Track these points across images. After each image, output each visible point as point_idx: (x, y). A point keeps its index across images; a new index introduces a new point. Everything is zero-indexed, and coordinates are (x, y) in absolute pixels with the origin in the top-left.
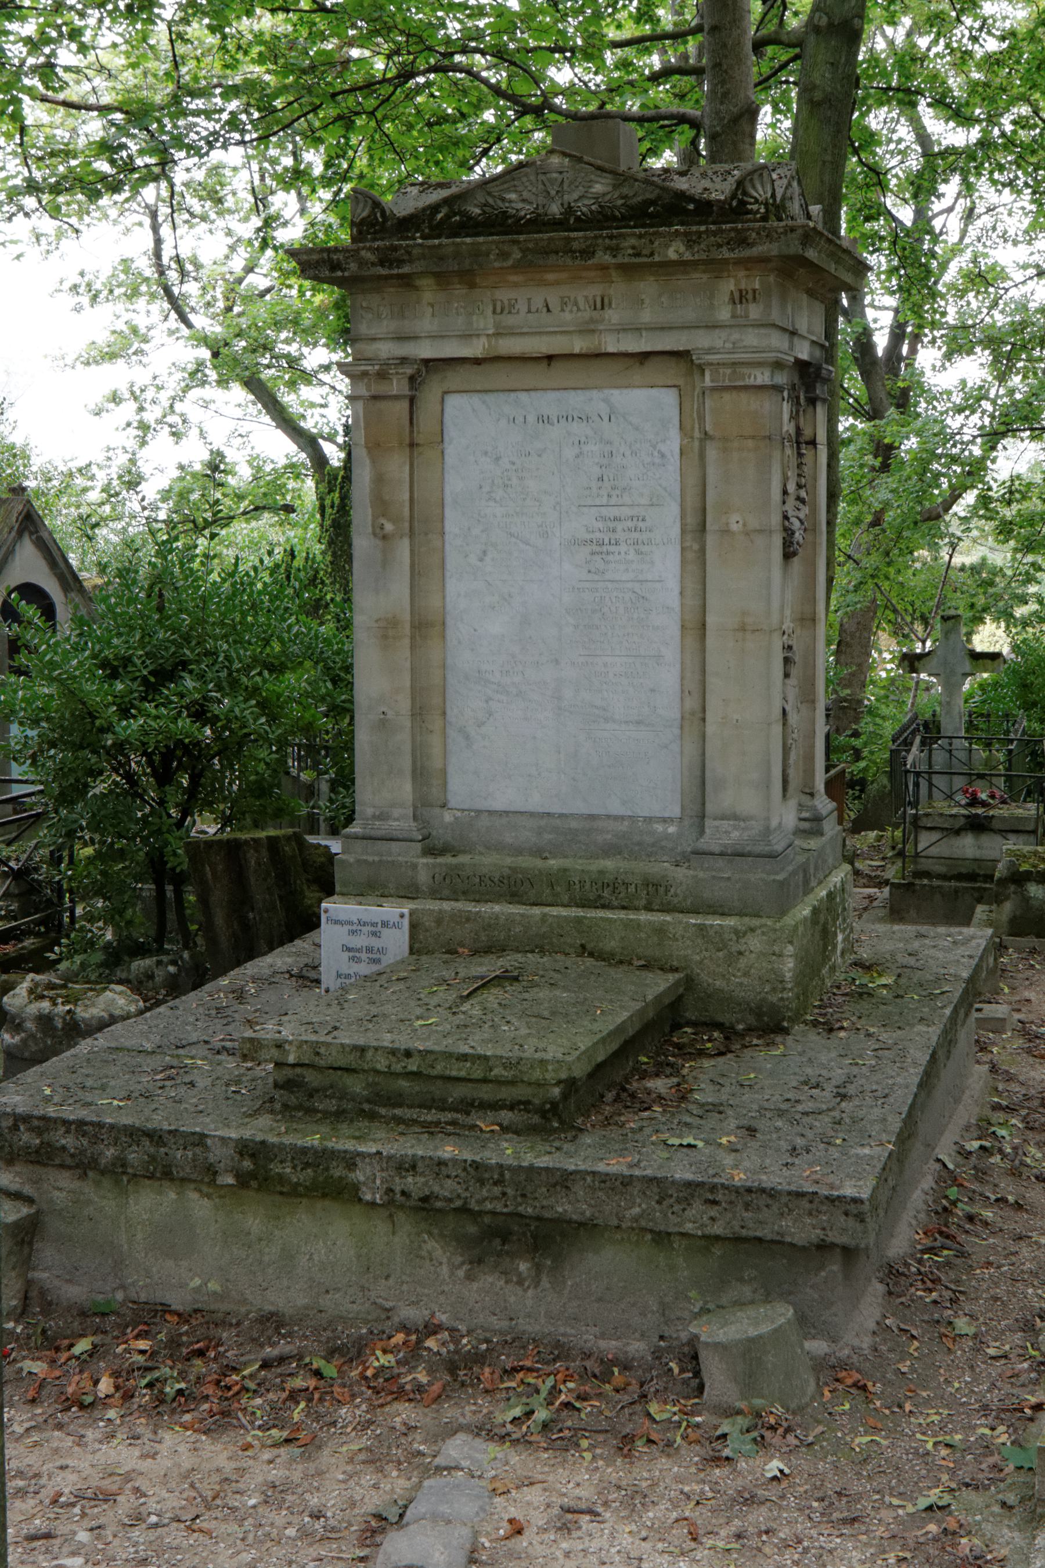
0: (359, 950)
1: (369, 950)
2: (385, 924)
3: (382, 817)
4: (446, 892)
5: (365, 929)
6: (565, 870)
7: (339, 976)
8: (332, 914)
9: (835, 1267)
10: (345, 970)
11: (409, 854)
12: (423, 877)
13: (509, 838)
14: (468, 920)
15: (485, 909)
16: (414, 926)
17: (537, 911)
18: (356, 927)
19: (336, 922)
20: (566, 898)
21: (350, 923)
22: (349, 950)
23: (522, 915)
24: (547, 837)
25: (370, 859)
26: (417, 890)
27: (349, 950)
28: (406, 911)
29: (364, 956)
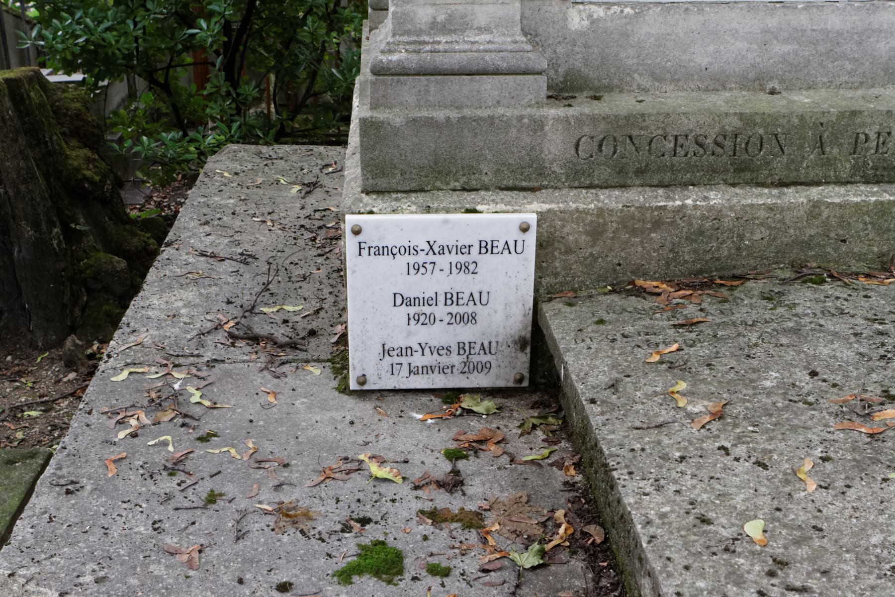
0: (427, 302)
1: (452, 298)
2: (487, 247)
3: (452, 25)
4: (603, 173)
5: (443, 261)
6: (854, 113)
7: (386, 351)
8: (370, 237)
9: (335, 384)
10: (399, 341)
11: (523, 100)
12: (555, 147)
13: (701, 56)
14: (657, 224)
15: (690, 199)
16: (545, 246)
17: (796, 197)
18: (421, 257)
19: (381, 251)
20: (845, 168)
21: (409, 250)
22: (408, 302)
23: (770, 208)
24: (779, 49)
25: (440, 115)
26: (541, 172)
27: (408, 302)
28: (532, 218)
29: (441, 311)
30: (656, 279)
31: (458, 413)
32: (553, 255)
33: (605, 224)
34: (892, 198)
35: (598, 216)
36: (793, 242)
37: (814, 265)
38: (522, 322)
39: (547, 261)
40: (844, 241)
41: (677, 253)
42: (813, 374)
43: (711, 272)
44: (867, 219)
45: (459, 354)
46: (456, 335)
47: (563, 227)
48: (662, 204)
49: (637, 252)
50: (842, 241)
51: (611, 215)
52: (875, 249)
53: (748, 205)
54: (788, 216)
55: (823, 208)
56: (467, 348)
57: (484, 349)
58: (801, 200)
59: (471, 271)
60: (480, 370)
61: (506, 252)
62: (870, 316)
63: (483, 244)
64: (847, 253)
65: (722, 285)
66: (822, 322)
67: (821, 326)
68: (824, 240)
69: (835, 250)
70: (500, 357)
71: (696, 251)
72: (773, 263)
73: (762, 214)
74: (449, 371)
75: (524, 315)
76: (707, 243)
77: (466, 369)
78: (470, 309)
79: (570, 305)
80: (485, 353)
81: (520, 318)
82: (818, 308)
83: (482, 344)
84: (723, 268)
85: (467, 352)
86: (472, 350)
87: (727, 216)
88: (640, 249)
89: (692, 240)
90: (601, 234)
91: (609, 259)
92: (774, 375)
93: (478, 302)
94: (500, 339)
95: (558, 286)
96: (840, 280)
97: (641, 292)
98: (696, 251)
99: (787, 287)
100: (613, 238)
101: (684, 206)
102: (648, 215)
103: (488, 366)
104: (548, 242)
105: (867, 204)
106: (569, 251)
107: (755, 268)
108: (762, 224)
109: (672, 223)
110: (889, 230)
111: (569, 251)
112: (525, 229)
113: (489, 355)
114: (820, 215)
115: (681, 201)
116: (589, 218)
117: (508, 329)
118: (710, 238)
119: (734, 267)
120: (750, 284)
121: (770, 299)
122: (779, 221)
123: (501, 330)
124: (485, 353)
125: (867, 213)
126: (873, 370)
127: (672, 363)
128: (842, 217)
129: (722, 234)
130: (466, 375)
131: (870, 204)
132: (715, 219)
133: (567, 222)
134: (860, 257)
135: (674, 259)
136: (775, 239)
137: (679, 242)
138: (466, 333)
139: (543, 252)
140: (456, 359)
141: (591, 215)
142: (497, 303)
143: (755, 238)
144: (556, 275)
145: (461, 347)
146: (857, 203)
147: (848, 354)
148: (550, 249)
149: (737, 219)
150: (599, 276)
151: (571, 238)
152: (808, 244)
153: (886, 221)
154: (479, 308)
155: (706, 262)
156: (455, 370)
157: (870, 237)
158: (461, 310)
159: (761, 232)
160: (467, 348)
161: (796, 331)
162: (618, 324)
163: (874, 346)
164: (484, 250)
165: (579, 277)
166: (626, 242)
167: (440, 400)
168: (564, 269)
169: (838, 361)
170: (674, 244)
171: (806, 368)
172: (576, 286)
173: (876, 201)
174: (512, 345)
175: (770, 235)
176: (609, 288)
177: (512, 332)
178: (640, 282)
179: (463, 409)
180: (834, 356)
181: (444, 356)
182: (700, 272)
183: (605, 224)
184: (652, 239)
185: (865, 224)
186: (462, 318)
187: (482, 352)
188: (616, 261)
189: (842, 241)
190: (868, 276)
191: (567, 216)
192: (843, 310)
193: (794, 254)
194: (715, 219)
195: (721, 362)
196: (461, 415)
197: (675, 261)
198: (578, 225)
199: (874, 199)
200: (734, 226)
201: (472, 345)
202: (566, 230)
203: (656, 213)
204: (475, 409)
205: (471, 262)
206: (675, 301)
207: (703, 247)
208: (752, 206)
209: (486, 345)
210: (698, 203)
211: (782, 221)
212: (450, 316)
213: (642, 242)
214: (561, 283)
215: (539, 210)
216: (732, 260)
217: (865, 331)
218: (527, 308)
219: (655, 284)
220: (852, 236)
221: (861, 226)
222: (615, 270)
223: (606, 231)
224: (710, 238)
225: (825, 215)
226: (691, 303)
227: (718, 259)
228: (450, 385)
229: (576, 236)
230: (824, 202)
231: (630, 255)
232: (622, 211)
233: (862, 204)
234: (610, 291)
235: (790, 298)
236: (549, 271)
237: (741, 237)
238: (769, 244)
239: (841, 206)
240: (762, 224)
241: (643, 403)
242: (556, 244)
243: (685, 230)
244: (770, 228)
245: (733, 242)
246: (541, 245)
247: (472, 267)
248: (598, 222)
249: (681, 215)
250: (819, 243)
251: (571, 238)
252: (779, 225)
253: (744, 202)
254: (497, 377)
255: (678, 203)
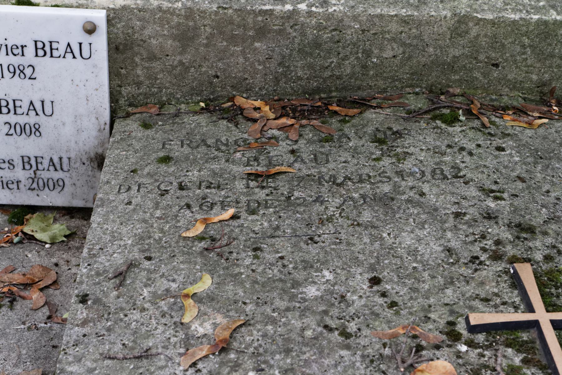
2: (44, 49)
14: (262, 32)
23: (405, 21)
30: (258, 96)
31: (16, 240)
32: (133, 61)
33: (196, 28)
34: (558, 18)
35: (187, 17)
36: (432, 62)
37: (458, 91)
38: (96, 137)
39: (126, 68)
40: (496, 65)
41: (288, 67)
42: (375, 281)
43: (331, 92)
44: (526, 41)
45: (24, 169)
46: (17, 148)
47: (143, 28)
48: (268, 7)
49: (237, 62)
50: (493, 65)
51: (204, 18)
52: (535, 77)
53: (377, 16)
54: (427, 32)
55: (471, 24)
56: (33, 162)
57: (54, 165)
58: (444, 13)
59: (28, 76)
60: (51, 187)
61: (69, 56)
62: (489, 185)
63: (40, 45)
64: (499, 80)
65: (336, 113)
66: (426, 188)
67: (422, 194)
68: (471, 63)
69: (485, 75)
70: (74, 174)
71: (311, 66)
72: (407, 86)
73: (394, 27)
74: (15, 186)
75: (99, 130)
76: (325, 58)
77: (35, 185)
78: (32, 119)
79: (146, 126)
80: (56, 170)
81: (94, 133)
82: (431, 162)
83: (51, 160)
84: (345, 88)
85: (34, 167)
86: (39, 165)
87: (350, 27)
88: (241, 60)
89: (307, 53)
90: (192, 39)
91: (204, 69)
92: (328, 275)
93: (40, 112)
94: (73, 155)
95: (141, 97)
96: (478, 118)
97: (235, 115)
98: (311, 66)
99: (408, 125)
100: (207, 46)
101: (295, 12)
102: (250, 20)
103: (61, 183)
104: (126, 45)
105: (527, 22)
106: (152, 57)
107: (385, 91)
108: (394, 39)
109: (281, 32)
110: (552, 56)
111: (152, 57)
112: (90, 29)
113: (61, 172)
114: (467, 33)
115: (292, 4)
116: (176, 19)
117: (81, 144)
118: (329, 52)
119: (359, 88)
120: (370, 114)
121: (381, 142)
122: (415, 37)
123: (73, 144)
124: (56, 170)
125: (526, 34)
126: (452, 283)
127: (213, 239)
128: (495, 36)
129: (344, 48)
130: (35, 192)
131: (530, 23)
132: (335, 30)
133: (148, 22)
134: (514, 86)
135: (284, 74)
136: (410, 58)
137: (290, 55)
138: (30, 146)
139: (120, 57)
140: (20, 174)
141: (178, 15)
142: (64, 113)
143: (385, 56)
144: (139, 84)
145: (26, 161)
146: (514, 22)
147: (432, 249)
148: (129, 54)
149: (363, 31)
150: (193, 89)
151: (154, 42)
152: (451, 67)
153: (550, 45)
154: (42, 119)
155: (325, 80)
156: (21, 186)
157: (529, 62)
158: (22, 120)
159: (393, 49)
160: (33, 162)
161: (386, 202)
162: (184, 165)
163: (471, 238)
164: (41, 53)
165: (167, 88)
166: (224, 51)
167: (6, 218)
168: (149, 78)
169: (416, 261)
170: (284, 57)
171: (372, 268)
172: (164, 98)
173: (538, 20)
174: (87, 163)
175: (404, 53)
176: (202, 104)
177: (87, 148)
178: (240, 101)
179: (25, 234)
180: (416, 250)
181: (7, 169)
182: (313, 92)
183: (196, 28)
184: (256, 49)
185: (523, 46)
186: (23, 129)
187: (52, 168)
188: (212, 72)
189: (493, 65)
190: (520, 111)
191: (147, 15)
192: (460, 170)
193: (433, 77)
194: (335, 30)
195: (273, 245)
196: (20, 242)
197: (285, 76)
198: (162, 26)
199: (536, 17)
200: (358, 40)
201: (39, 160)
202: (147, 32)
203: (260, 18)
204: (38, 236)
205: (26, 65)
206: (271, 133)
207: (320, 62)
208: (381, 16)
209: (56, 160)
210: (314, 9)
211: (419, 37)
212: (8, 126)
213: (243, 52)
214: (146, 94)
215: (112, 6)
216: (356, 79)
217: (471, 211)
218: (102, 123)
219: (258, 103)
220: (506, 60)
221: (518, 49)
222: (211, 83)
223: (198, 36)
224: (329, 52)
225: (474, 32)
226: (287, 138)
227: (339, 78)
228: (18, 202)
229: (160, 40)
230: (473, 17)
231: (229, 66)
232: (216, 13)
233: (521, 22)
234: (202, 109)
235: (406, 144)
236: (130, 79)
237: (368, 54)
238: (402, 64)
239: (494, 24)
240: (394, 39)
241: (143, 310)
242: (136, 49)
243: (297, 41)
244: (404, 44)
245: (358, 58)
246: (116, 49)
247: (28, 71)
248: (187, 25)
249: (292, 22)
250: (464, 66)
251: (154, 42)
252: (415, 42)
253: (371, 11)
254: (73, 196)
255: (288, 7)
